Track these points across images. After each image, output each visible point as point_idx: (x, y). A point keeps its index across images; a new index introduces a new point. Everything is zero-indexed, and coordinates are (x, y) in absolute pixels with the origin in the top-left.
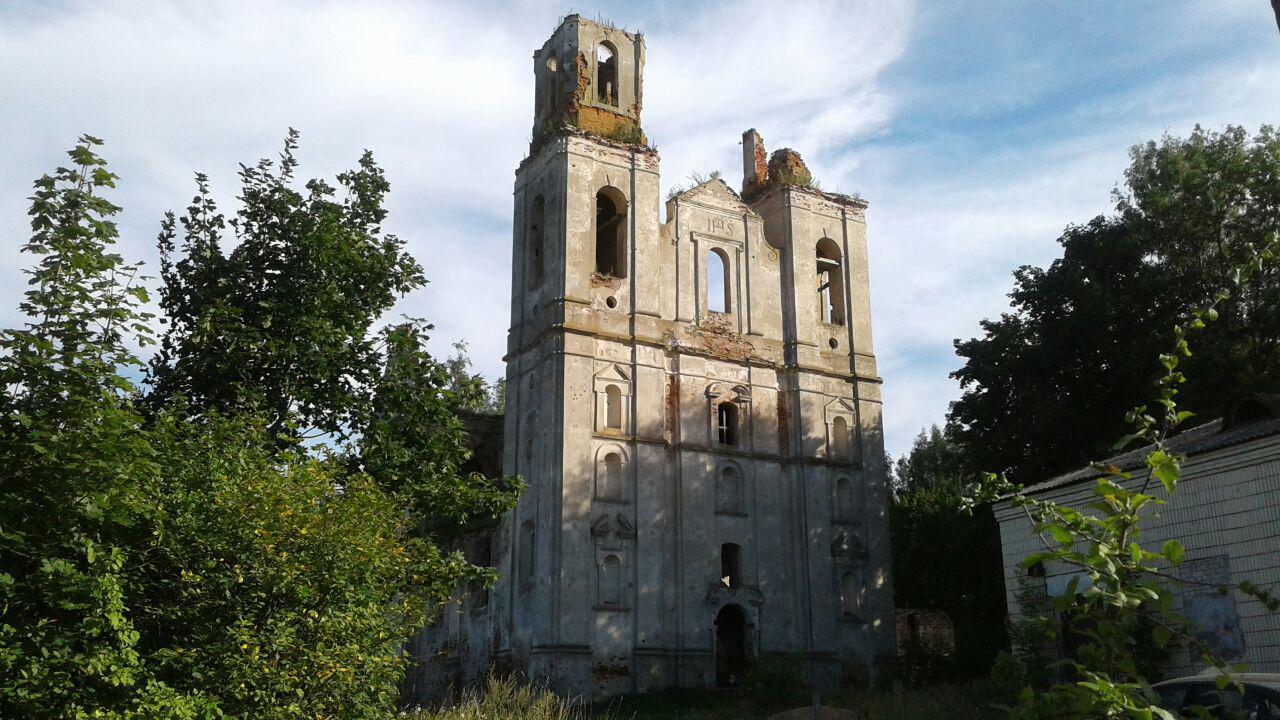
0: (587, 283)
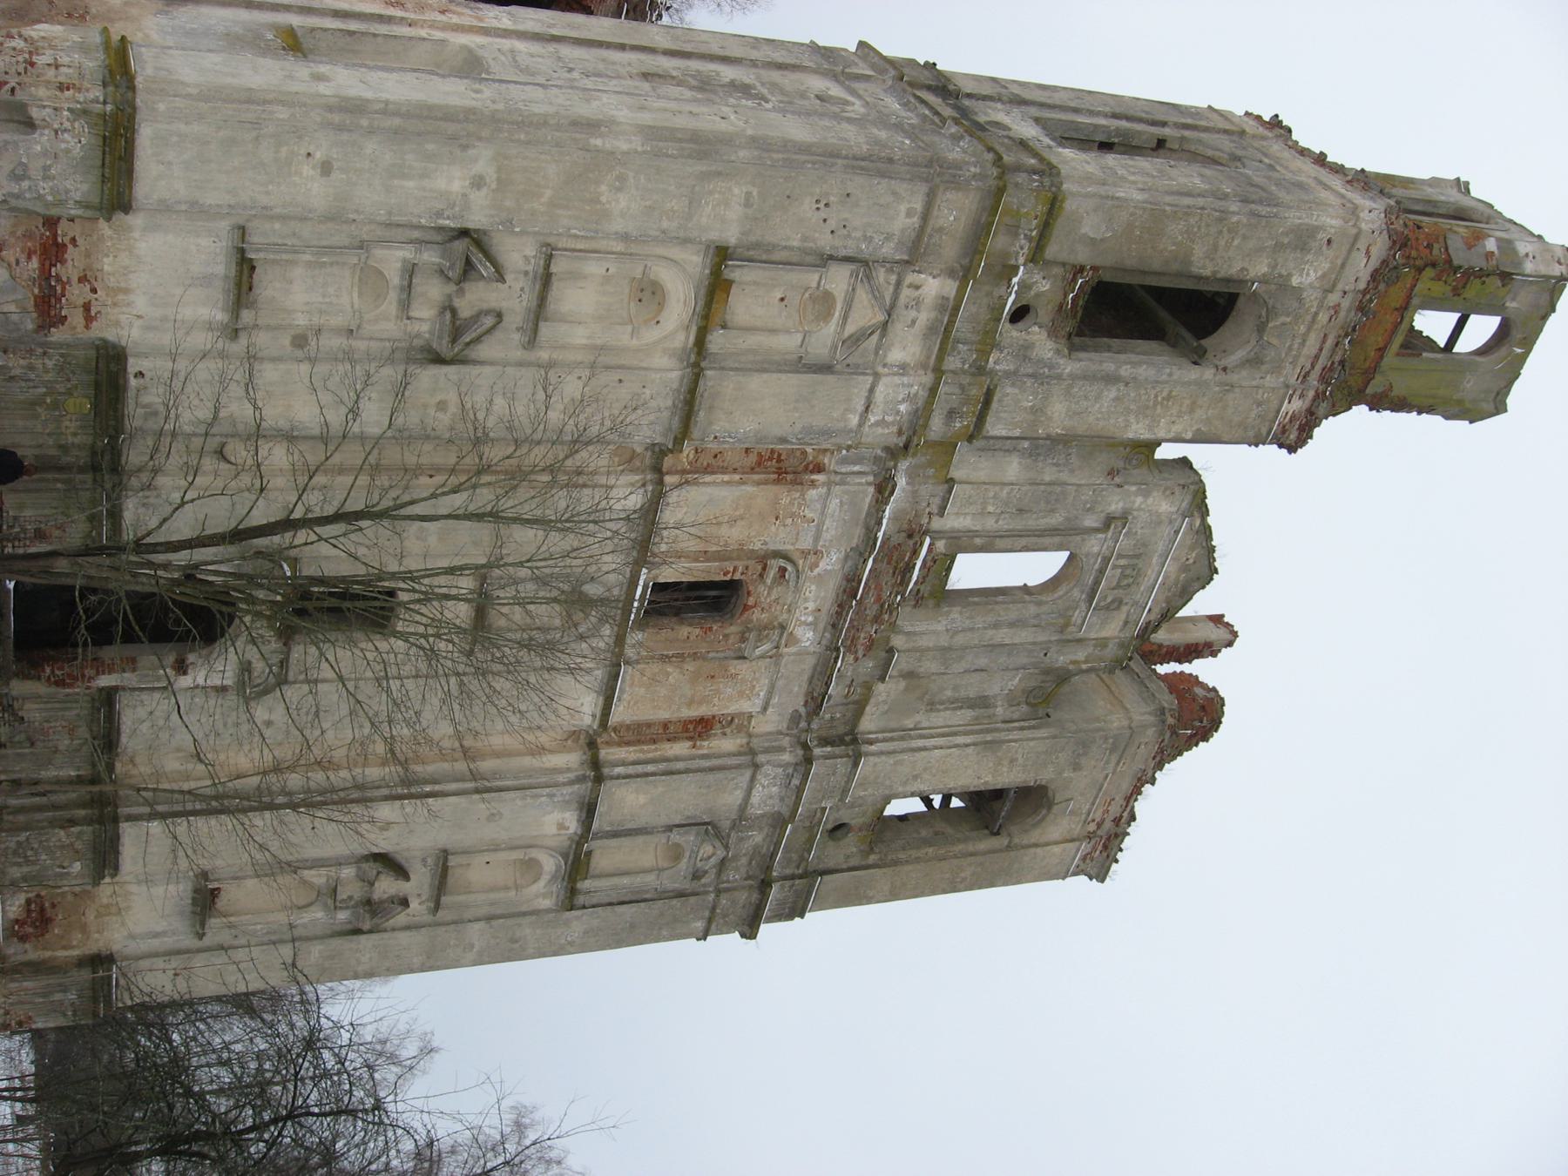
0: (1083, 256)
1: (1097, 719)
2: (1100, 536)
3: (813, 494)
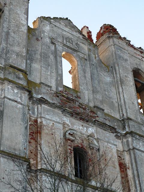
1: (112, 54)
2: (57, 46)
3: (44, 123)
